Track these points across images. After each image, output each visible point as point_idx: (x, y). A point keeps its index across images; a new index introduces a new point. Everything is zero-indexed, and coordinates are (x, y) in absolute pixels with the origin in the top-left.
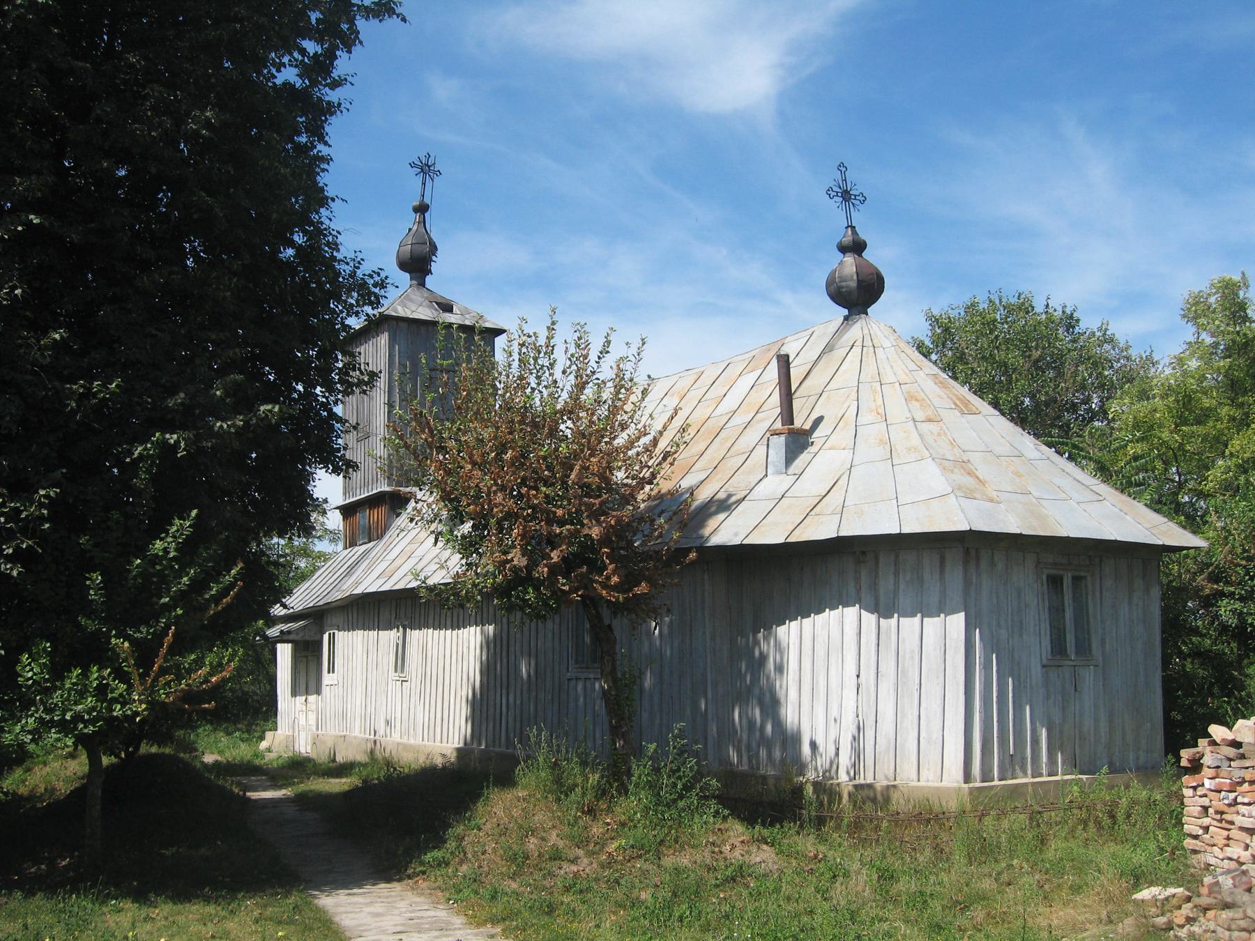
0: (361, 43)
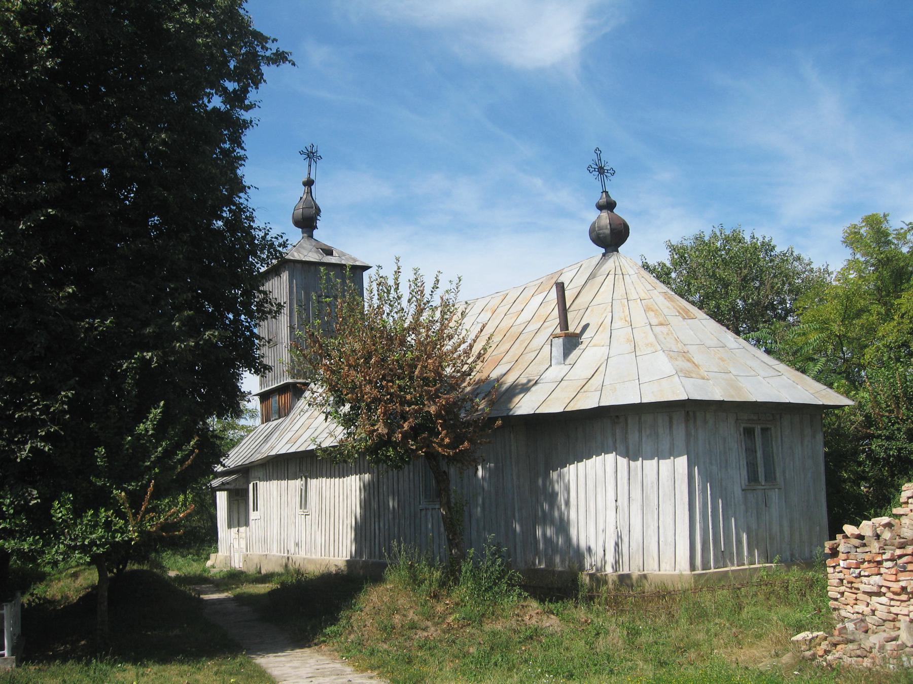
0: (265, 81)
